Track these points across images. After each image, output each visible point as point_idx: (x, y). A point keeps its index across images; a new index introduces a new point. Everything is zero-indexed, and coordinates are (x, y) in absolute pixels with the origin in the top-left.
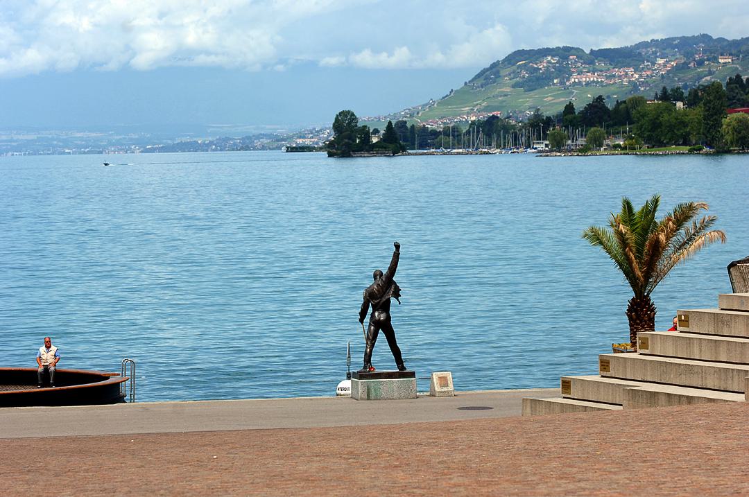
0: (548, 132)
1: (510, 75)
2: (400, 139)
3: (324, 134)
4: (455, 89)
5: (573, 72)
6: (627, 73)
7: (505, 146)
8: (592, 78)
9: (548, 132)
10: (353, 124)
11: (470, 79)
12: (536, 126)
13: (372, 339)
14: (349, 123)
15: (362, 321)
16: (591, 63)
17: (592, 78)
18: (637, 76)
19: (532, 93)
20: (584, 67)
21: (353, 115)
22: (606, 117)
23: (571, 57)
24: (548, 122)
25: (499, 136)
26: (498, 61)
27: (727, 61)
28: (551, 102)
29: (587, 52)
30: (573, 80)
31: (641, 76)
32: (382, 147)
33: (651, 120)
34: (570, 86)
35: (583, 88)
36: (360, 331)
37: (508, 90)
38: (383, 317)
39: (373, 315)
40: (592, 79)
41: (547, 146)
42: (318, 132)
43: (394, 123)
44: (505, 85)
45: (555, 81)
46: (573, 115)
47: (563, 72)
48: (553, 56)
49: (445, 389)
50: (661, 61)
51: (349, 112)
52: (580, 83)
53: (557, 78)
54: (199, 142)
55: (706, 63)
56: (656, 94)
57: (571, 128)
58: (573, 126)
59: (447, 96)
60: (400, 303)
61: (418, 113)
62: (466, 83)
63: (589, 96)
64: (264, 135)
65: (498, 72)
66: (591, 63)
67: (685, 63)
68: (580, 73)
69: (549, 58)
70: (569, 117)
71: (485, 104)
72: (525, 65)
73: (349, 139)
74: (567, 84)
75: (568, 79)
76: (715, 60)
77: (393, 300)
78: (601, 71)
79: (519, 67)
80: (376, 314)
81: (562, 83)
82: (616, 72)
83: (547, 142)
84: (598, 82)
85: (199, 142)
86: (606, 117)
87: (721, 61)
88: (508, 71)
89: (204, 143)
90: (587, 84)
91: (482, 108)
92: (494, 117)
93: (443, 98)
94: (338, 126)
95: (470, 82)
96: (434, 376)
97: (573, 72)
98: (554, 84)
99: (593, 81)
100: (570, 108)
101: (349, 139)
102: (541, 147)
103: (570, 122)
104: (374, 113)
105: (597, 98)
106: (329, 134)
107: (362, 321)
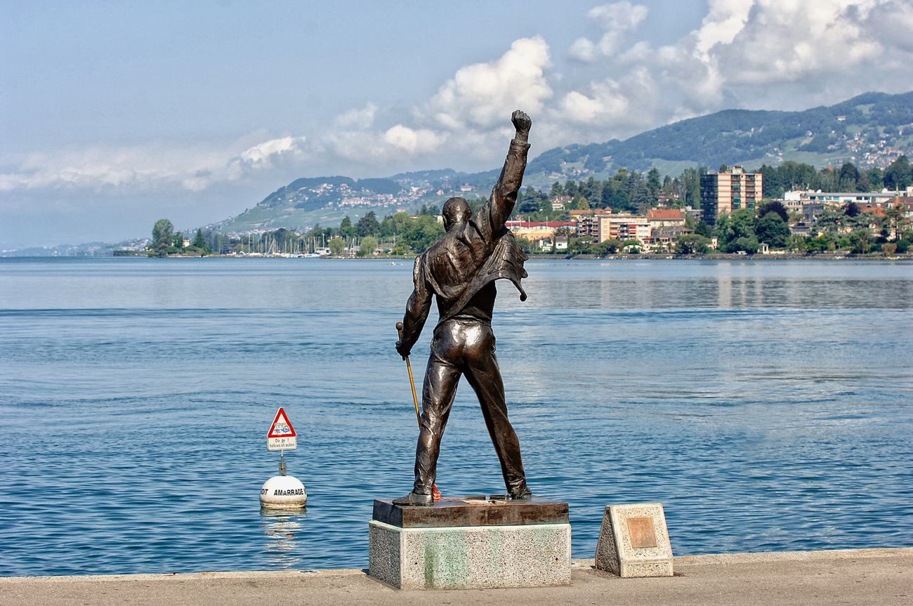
0: (329, 241)
1: (293, 198)
2: (206, 244)
3: (143, 243)
4: (249, 208)
5: (345, 197)
6: (387, 199)
7: (293, 251)
8: (360, 201)
9: (329, 241)
10: (169, 231)
11: (262, 200)
12: (319, 236)
13: (437, 403)
14: (166, 231)
15: (404, 349)
16: (359, 189)
17: (360, 201)
18: (395, 201)
19: (311, 213)
20: (353, 193)
21: (169, 223)
22: (376, 229)
23: (343, 185)
24: (329, 233)
25: (288, 243)
26: (284, 187)
27: (468, 189)
28: (329, 219)
29: (356, 181)
30: (344, 203)
31: (398, 201)
32: (192, 250)
33: (416, 231)
34: (341, 207)
35: (354, 206)
36: (405, 379)
37: (292, 210)
38: (472, 336)
39: (441, 334)
40: (359, 202)
41: (328, 251)
42: (138, 241)
43: (203, 231)
44: (290, 206)
45: (330, 203)
46: (349, 227)
47: (335, 196)
48: (328, 184)
49: (648, 555)
50: (415, 189)
51: (166, 221)
52: (349, 205)
53: (330, 201)
54: (45, 248)
55: (451, 191)
56: (417, 212)
57: (348, 237)
58: (350, 235)
59: (243, 214)
60: (523, 298)
61: (219, 227)
62: (258, 204)
63: (357, 216)
64: (96, 244)
65: (284, 195)
66: (359, 189)
67: (433, 191)
68: (350, 197)
69: (325, 185)
70: (346, 228)
71: (273, 221)
72: (306, 190)
73: (166, 243)
74: (339, 206)
75: (340, 202)
76: (458, 188)
77: (504, 287)
78: (366, 196)
79: (301, 191)
80: (455, 328)
81: (335, 205)
82: (380, 197)
83: (328, 249)
84: (363, 205)
85: (45, 248)
86: (376, 229)
87: (463, 190)
88: (291, 195)
89: (48, 249)
90: (356, 206)
91: (271, 224)
92: (282, 230)
93: (240, 215)
94: (156, 233)
95: (261, 203)
96: (616, 517)
97: (345, 197)
98: (328, 206)
99: (360, 204)
100: (346, 222)
101: (165, 244)
102: (323, 252)
103: (347, 232)
104: (186, 225)
105: (369, 214)
106: (149, 238)
107: (404, 349)
